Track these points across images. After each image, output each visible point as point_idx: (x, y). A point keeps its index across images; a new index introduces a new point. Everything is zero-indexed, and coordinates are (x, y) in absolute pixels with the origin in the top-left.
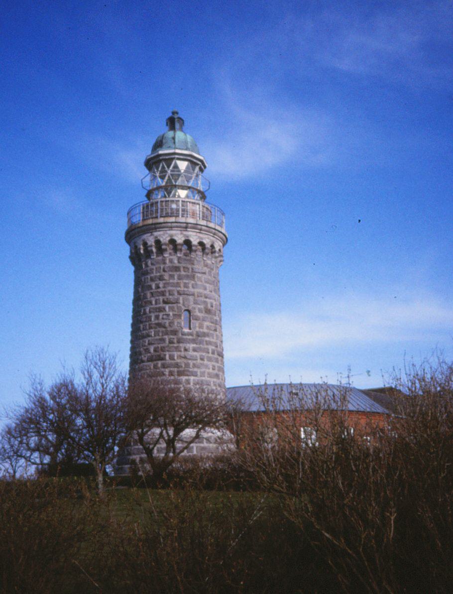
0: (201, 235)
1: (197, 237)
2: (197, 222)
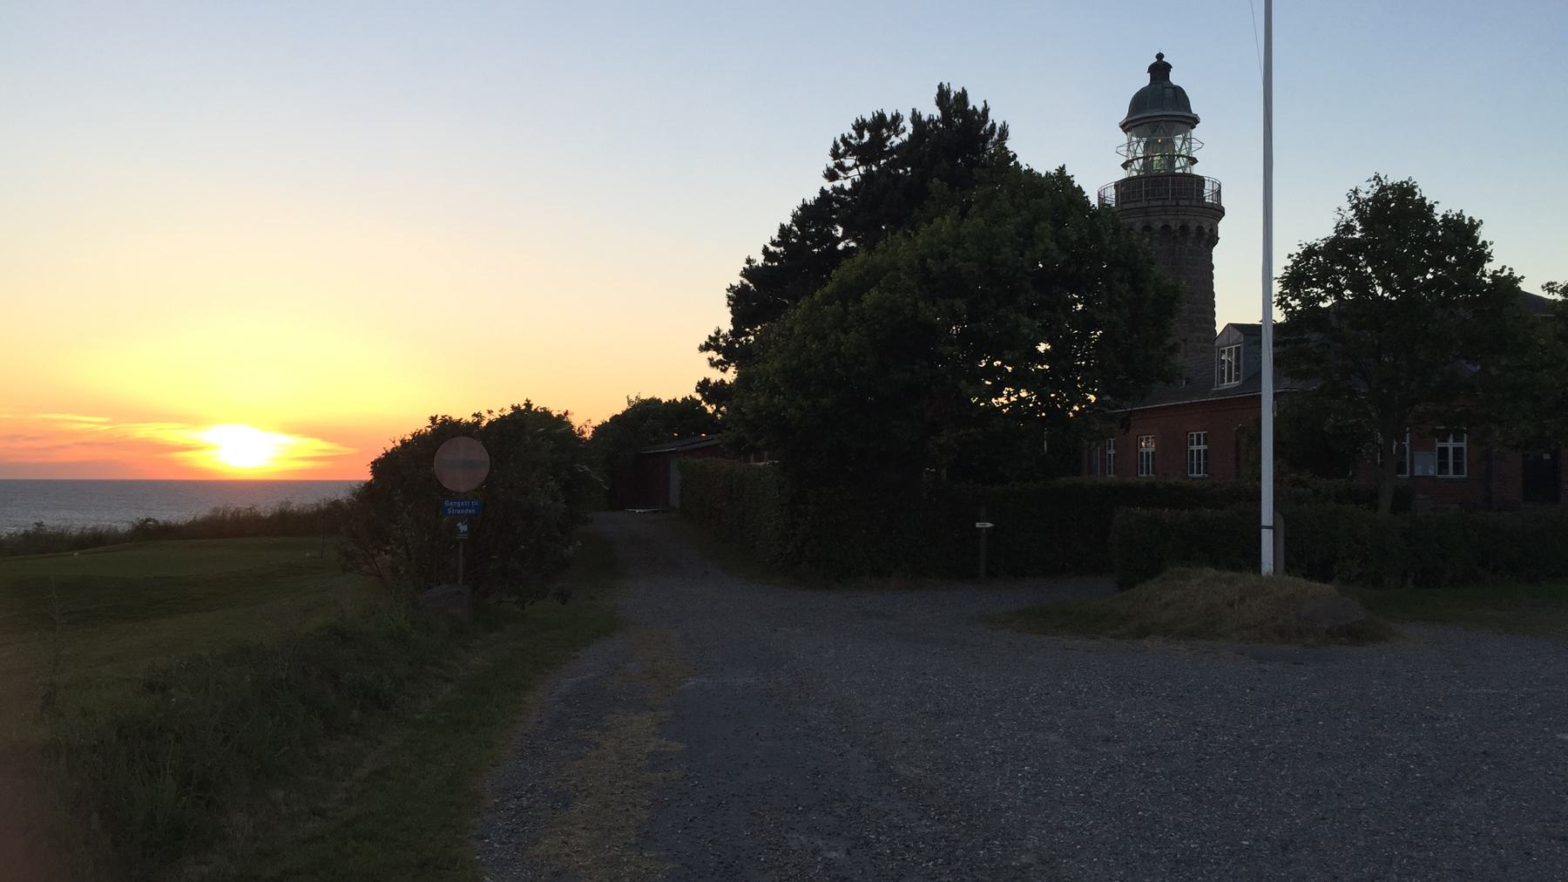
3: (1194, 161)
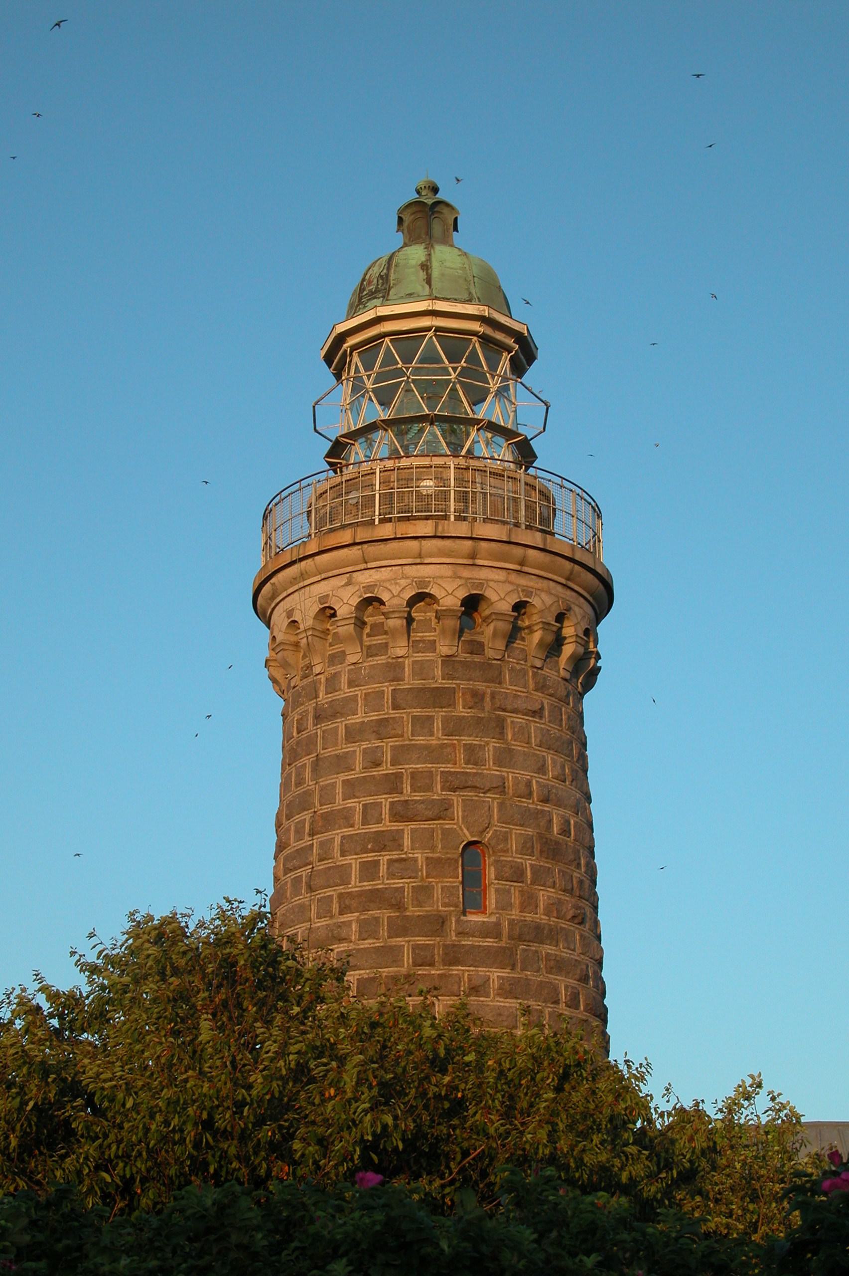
1: (510, 588)
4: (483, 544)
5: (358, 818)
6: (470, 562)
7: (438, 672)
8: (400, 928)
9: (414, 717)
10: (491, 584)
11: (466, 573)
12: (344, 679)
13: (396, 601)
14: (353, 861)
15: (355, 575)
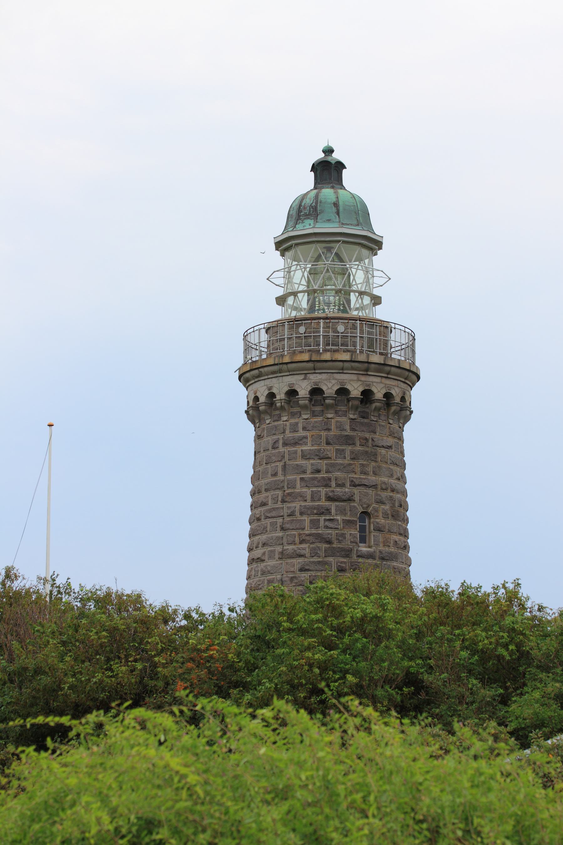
0: (388, 382)
2: (385, 361)
3: (376, 300)
4: (373, 365)
5: (309, 497)
6: (365, 373)
7: (348, 427)
8: (331, 552)
9: (337, 449)
10: (375, 384)
11: (363, 378)
12: (300, 426)
13: (329, 391)
14: (307, 519)
15: (308, 375)
